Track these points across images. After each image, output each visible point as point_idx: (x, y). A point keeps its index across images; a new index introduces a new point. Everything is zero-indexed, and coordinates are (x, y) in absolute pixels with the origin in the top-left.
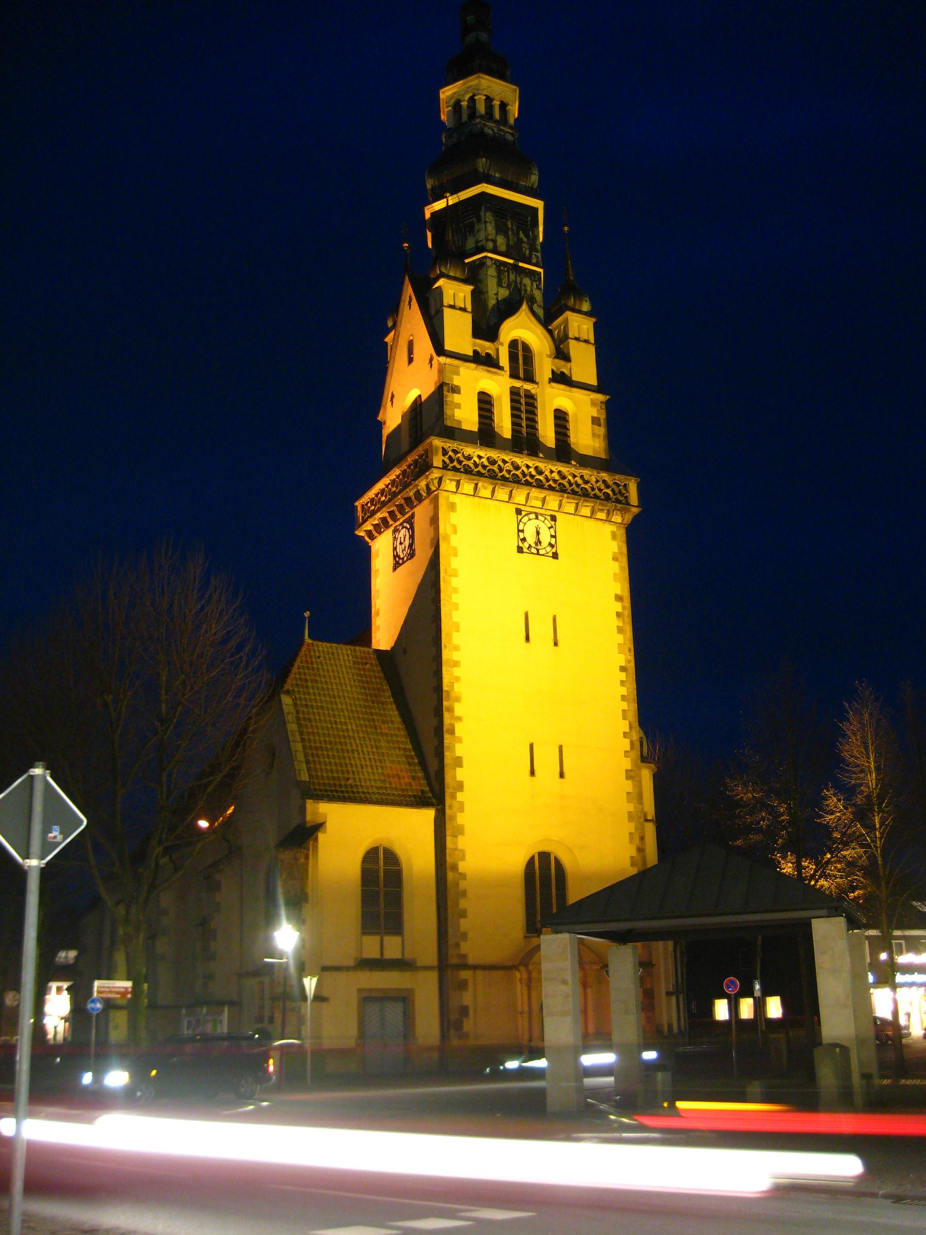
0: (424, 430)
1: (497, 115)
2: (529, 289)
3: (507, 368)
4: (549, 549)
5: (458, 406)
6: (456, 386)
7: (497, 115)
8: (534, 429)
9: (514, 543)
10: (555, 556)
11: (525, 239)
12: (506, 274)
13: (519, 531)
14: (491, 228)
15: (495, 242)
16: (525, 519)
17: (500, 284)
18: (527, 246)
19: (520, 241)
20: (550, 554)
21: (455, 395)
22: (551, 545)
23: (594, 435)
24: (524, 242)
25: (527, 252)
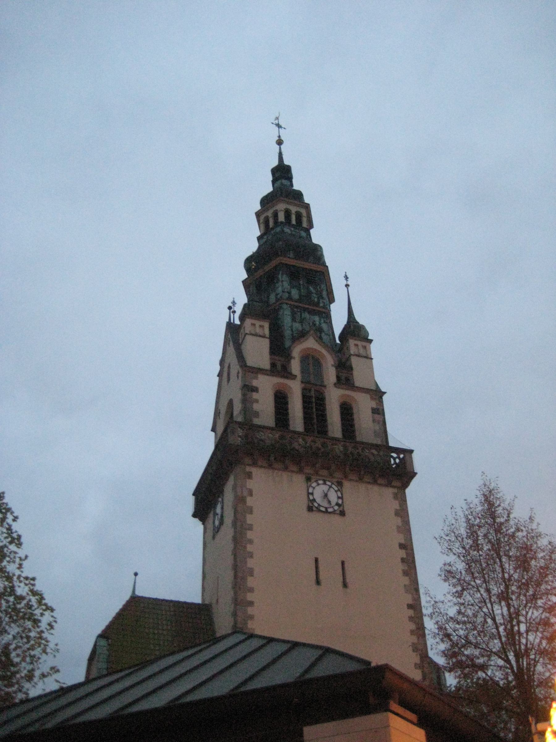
0: (528, 619)
1: (294, 222)
2: (317, 323)
3: (299, 377)
4: (336, 508)
5: (257, 401)
6: (254, 387)
7: (294, 222)
8: (287, 378)
9: (337, 518)
10: (342, 513)
11: (313, 291)
12: (299, 314)
13: (309, 494)
14: (286, 285)
15: (289, 293)
16: (314, 484)
17: (294, 320)
18: (315, 295)
19: (310, 293)
20: (338, 512)
21: (254, 394)
22: (337, 504)
23: (374, 421)
24: (313, 293)
25: (316, 300)
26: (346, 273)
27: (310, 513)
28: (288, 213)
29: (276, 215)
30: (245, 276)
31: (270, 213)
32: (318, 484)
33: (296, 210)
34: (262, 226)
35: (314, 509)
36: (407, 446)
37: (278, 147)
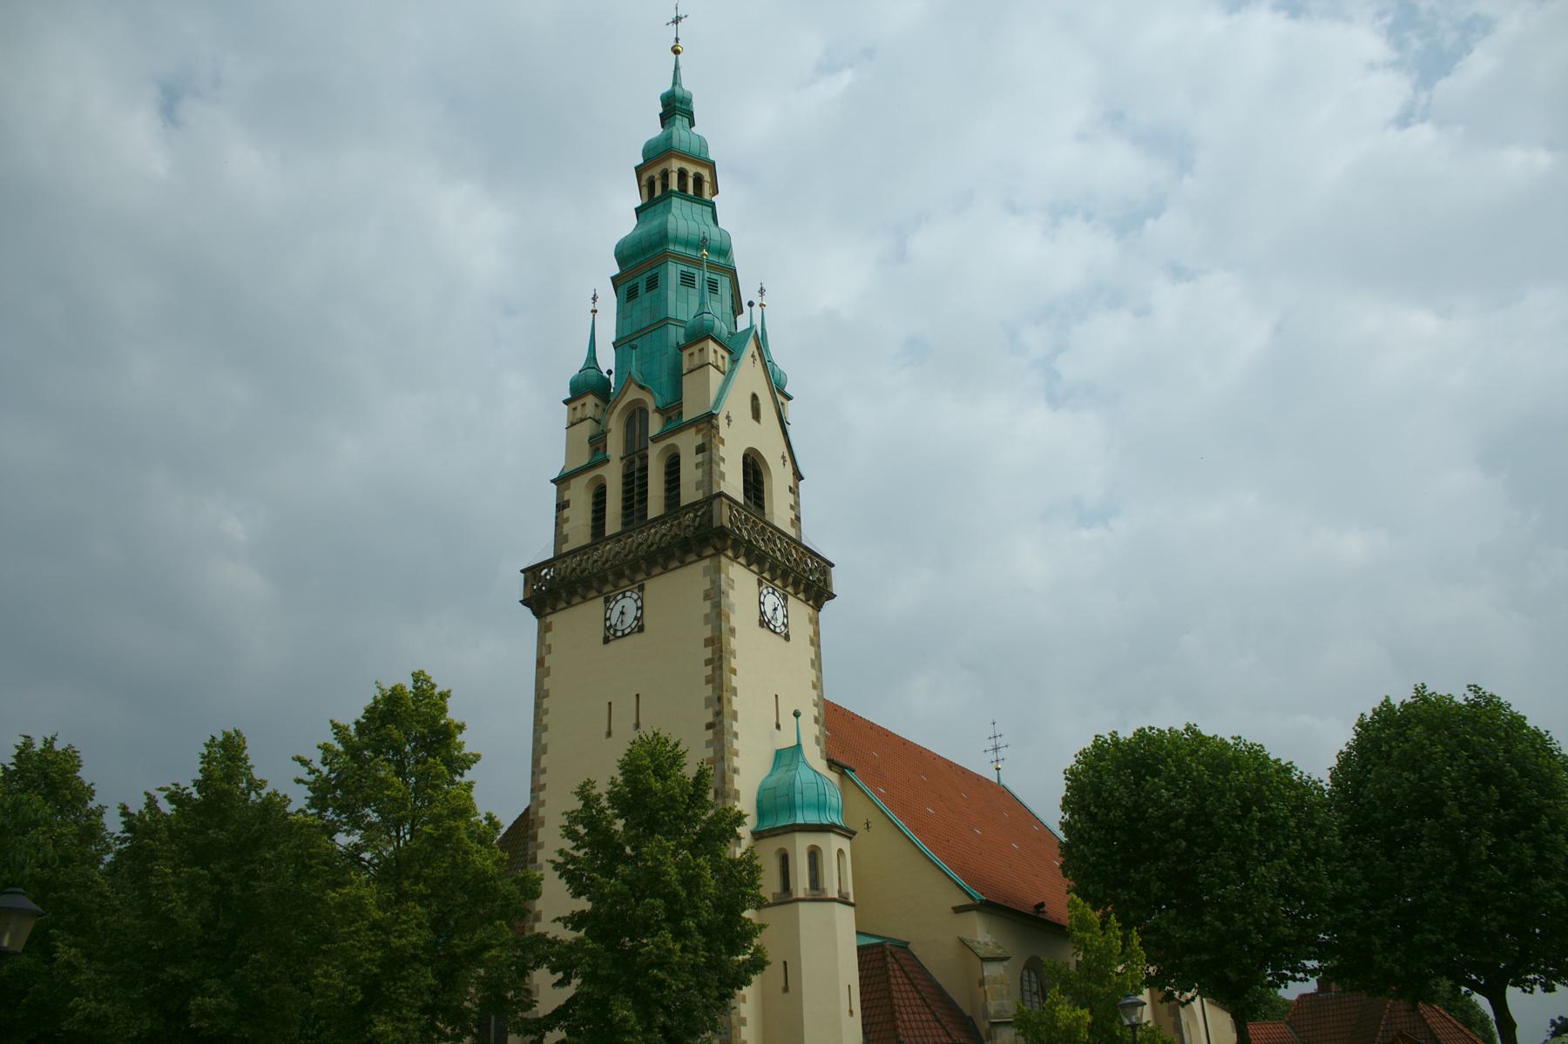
1: (691, 191)
9: (781, 641)
20: (783, 634)
26: (761, 284)
27: (646, 628)
28: (682, 174)
29: (665, 175)
30: (616, 270)
31: (656, 172)
32: (636, 601)
33: (695, 171)
34: (645, 190)
35: (640, 623)
36: (812, 544)
37: (674, 56)
